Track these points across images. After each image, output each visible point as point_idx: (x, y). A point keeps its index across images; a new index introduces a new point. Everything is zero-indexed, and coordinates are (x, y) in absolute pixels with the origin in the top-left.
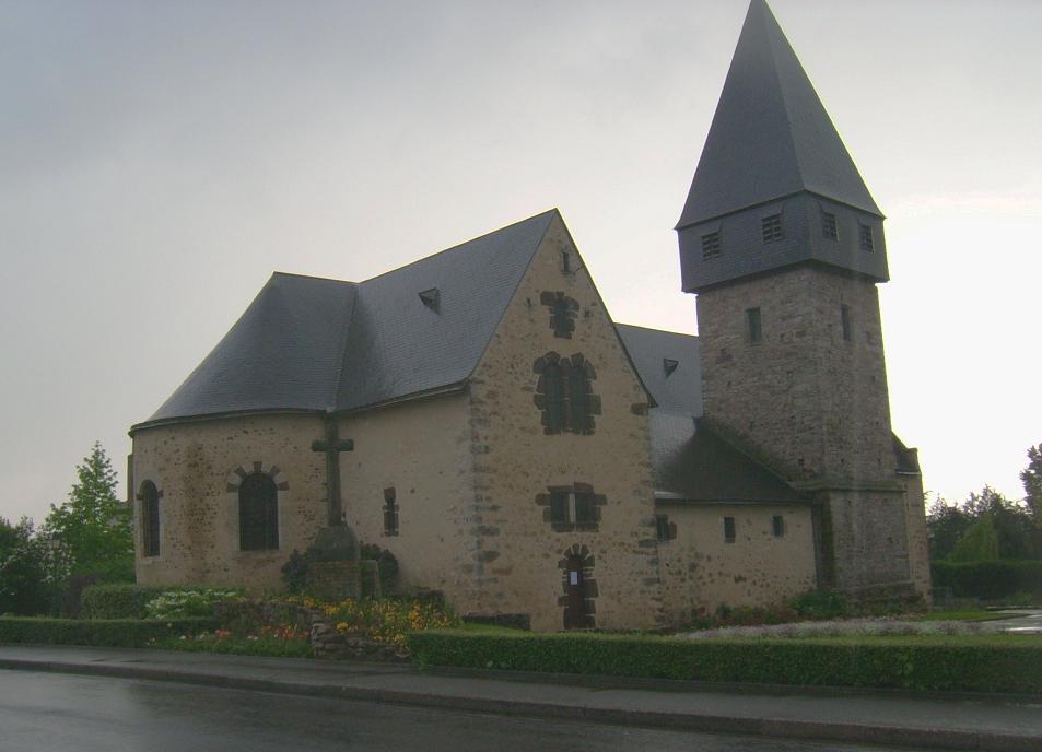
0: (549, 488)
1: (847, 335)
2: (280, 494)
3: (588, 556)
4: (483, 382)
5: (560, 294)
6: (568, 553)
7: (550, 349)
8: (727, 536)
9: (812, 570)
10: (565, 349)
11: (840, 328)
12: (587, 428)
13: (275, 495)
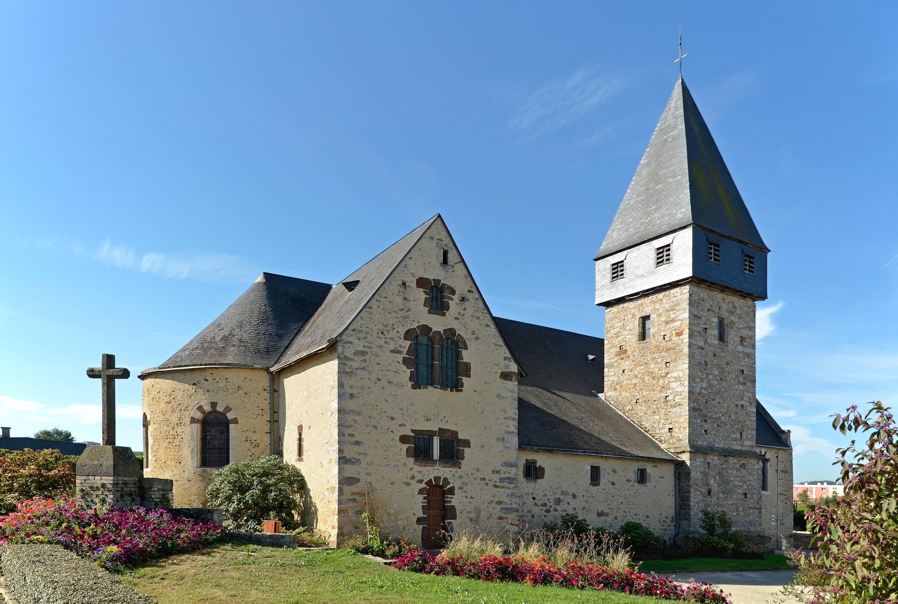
0: (413, 431)
1: (721, 338)
2: (232, 426)
3: (449, 487)
4: (350, 342)
5: (437, 281)
6: (429, 483)
7: (422, 322)
8: (592, 479)
9: (672, 513)
10: (438, 324)
11: (716, 332)
12: (457, 386)
13: (228, 427)
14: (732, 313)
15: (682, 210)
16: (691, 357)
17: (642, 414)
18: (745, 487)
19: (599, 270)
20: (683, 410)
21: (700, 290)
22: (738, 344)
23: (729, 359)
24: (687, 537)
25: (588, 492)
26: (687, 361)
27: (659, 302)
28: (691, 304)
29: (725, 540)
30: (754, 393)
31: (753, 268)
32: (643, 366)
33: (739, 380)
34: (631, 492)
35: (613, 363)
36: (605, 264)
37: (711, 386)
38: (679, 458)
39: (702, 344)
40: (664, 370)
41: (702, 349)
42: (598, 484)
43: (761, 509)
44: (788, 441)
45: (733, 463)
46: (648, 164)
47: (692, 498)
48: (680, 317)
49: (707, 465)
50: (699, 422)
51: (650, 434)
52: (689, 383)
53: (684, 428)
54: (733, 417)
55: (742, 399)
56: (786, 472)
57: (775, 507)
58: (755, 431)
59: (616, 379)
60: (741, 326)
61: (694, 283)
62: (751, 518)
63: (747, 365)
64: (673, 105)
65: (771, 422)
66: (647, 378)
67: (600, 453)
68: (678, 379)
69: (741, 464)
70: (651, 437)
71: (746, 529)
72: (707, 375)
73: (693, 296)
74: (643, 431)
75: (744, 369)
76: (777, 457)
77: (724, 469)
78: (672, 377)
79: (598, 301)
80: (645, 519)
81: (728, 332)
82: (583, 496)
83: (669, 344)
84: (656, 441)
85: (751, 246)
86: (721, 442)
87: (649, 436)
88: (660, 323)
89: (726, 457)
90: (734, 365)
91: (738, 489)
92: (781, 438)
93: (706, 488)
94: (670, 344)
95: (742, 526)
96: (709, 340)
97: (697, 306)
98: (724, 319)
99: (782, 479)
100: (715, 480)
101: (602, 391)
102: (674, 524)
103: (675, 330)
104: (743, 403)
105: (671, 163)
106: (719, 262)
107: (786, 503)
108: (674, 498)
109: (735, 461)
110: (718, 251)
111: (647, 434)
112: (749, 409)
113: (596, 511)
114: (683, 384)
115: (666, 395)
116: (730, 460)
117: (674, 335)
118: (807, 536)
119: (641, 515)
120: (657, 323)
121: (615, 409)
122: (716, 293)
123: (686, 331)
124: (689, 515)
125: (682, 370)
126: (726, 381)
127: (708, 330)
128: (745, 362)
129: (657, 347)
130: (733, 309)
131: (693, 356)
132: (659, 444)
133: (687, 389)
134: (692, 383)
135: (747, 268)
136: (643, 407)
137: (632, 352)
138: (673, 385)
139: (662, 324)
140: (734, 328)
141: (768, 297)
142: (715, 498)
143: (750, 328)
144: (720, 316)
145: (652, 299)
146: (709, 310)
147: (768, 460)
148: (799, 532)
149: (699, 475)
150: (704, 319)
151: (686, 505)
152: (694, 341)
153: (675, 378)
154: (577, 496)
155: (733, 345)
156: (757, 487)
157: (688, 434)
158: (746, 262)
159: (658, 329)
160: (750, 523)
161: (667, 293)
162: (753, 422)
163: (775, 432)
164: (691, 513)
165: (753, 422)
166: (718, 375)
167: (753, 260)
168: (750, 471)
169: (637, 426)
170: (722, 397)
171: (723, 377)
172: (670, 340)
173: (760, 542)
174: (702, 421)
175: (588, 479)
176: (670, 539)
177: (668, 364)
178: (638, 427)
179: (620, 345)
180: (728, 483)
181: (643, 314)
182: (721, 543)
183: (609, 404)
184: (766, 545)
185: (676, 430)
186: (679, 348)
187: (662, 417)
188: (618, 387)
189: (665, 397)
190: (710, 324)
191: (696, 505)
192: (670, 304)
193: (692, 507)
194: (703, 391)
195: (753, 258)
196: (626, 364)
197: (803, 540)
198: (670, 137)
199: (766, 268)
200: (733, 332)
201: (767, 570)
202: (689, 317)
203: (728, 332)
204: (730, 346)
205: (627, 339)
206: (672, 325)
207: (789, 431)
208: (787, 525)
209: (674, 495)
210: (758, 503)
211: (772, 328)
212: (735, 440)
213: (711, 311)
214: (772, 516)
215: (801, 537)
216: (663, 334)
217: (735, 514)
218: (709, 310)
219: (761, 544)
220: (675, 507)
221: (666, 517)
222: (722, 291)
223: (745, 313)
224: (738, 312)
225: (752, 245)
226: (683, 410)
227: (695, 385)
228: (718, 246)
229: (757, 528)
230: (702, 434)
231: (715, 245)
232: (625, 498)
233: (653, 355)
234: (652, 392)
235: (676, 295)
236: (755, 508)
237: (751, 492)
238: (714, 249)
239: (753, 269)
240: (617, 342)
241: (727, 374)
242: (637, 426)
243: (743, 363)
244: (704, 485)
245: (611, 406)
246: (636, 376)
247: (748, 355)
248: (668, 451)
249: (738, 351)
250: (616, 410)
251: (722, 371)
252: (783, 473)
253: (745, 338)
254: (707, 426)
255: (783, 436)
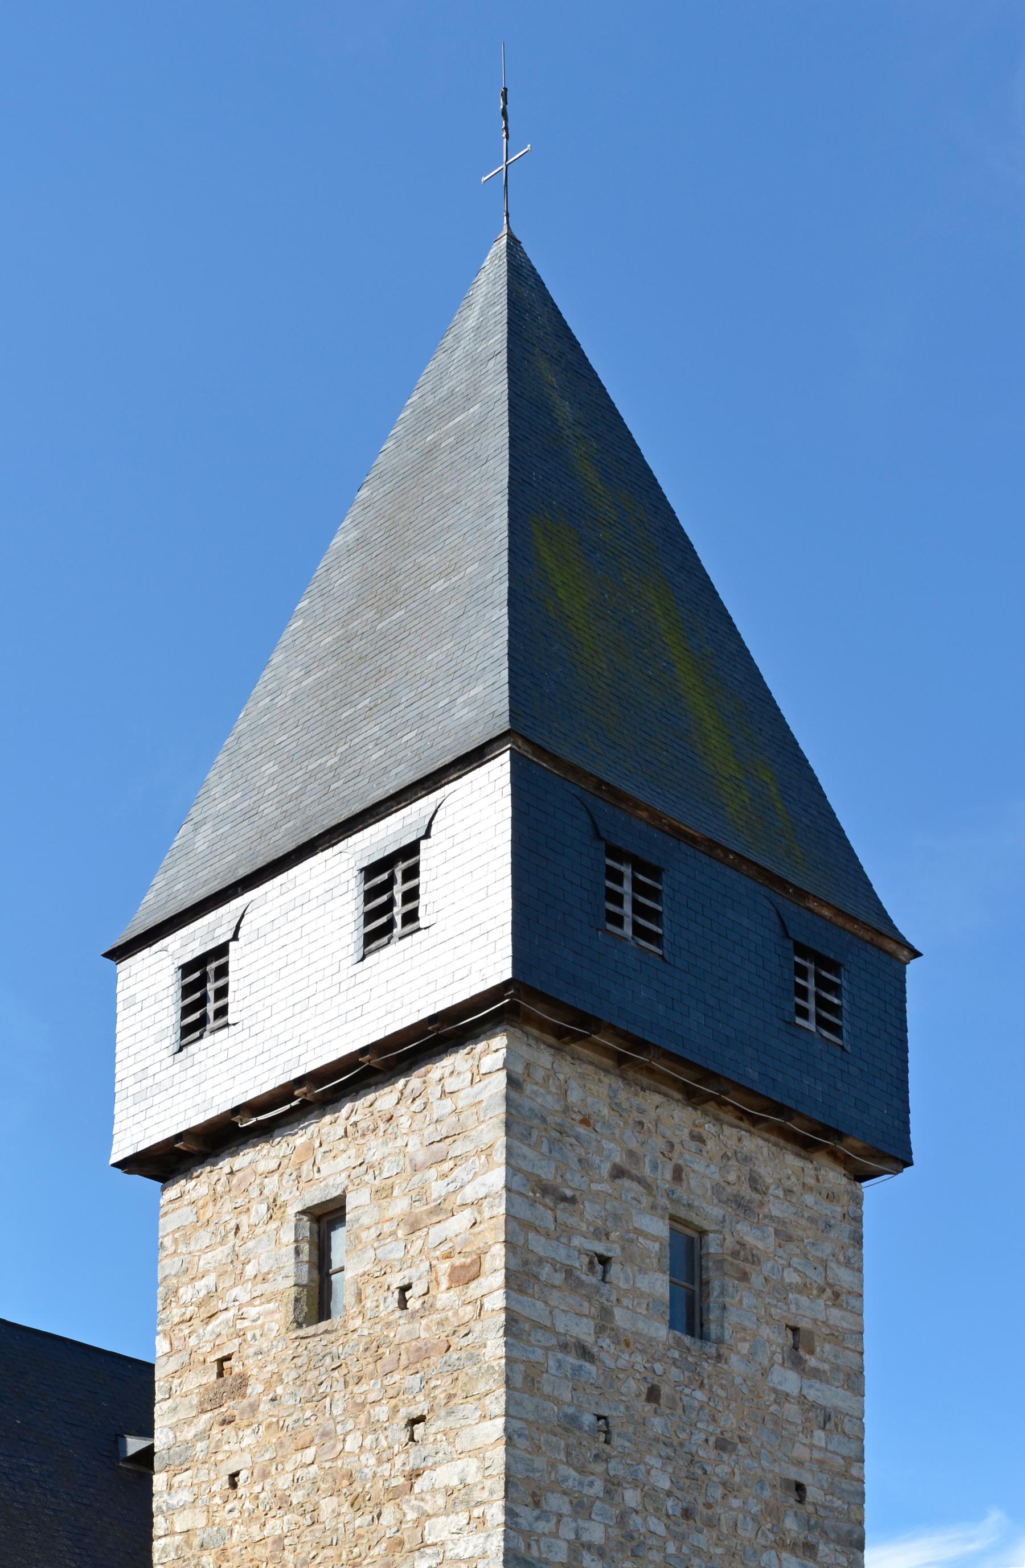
14: (742, 1206)
15: (472, 693)
16: (518, 1381)
21: (566, 1069)
22: (778, 1358)
23: (729, 1422)
26: (496, 1403)
27: (382, 1126)
31: (835, 1009)
33: (778, 1528)
35: (189, 1445)
39: (584, 1330)
40: (399, 1461)
41: (584, 1353)
46: (362, 542)
52: (509, 1512)
59: (201, 1521)
60: (791, 1277)
61: (535, 1032)
63: (821, 1463)
64: (471, 323)
72: (612, 1486)
73: (529, 1088)
75: (806, 1478)
78: (433, 1490)
81: (722, 1293)
83: (424, 1330)
88: (387, 1228)
90: (755, 1456)
94: (428, 1328)
96: (621, 1318)
97: (552, 1142)
98: (703, 1233)
103: (448, 1256)
106: (660, 946)
110: (653, 894)
114: (482, 1520)
117: (444, 1283)
120: (373, 1233)
122: (657, 1098)
123: (496, 1258)
125: (478, 1452)
126: (712, 1523)
127: (615, 1269)
128: (812, 1447)
129: (374, 1348)
131: (531, 1382)
134: (527, 1515)
135: (811, 1005)
137: (269, 1385)
138: (438, 1529)
139: (393, 1233)
140: (757, 1281)
141: (915, 1157)
143: (837, 1295)
144: (682, 1213)
145: (352, 1119)
150: (590, 1210)
152: (533, 1309)
153: (449, 1492)
155: (749, 1358)
158: (805, 998)
159: (377, 1261)
161: (414, 1081)
166: (669, 1494)
171: (700, 1507)
172: (427, 1308)
177: (419, 1429)
179: (219, 1355)
181: (315, 1196)
186: (464, 1342)
190: (627, 1243)
192: (426, 1132)
195: (834, 967)
200: (748, 1300)
202: (508, 1188)
203: (722, 1293)
204: (735, 1364)
206: (436, 1233)
216: (397, 1281)
218: (618, 1173)
222: (692, 1097)
223: (810, 1219)
224: (775, 1208)
225: (829, 905)
227: (542, 1526)
228: (655, 872)
233: (357, 1390)
235: (451, 1084)
238: (635, 882)
239: (839, 1016)
241: (718, 1493)
243: (801, 1452)
246: (283, 1502)
247: (828, 1418)
249: (775, 1390)
253: (810, 1333)
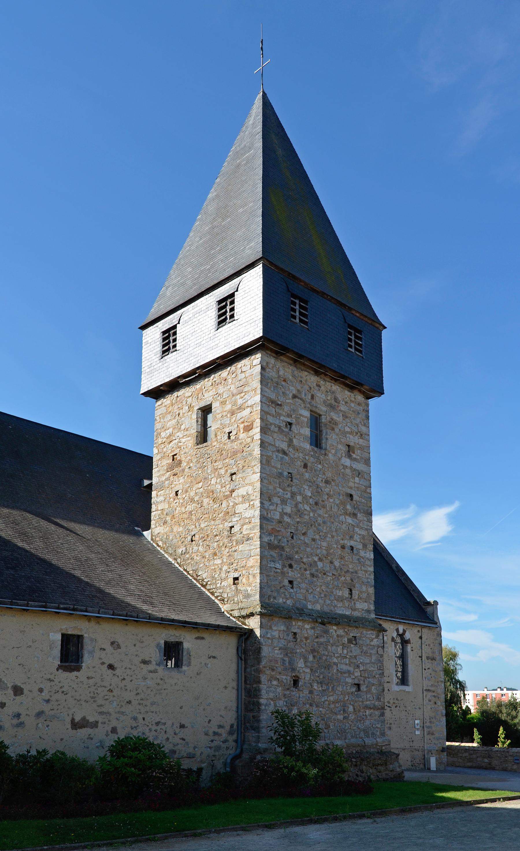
11: (307, 431)
14: (332, 407)
16: (264, 462)
17: (198, 558)
18: (357, 674)
19: (147, 343)
20: (253, 547)
21: (279, 364)
22: (344, 455)
23: (329, 475)
24: (252, 759)
25: (52, 683)
26: (258, 469)
27: (223, 382)
28: (263, 381)
29: (304, 763)
30: (370, 529)
31: (360, 345)
32: (201, 483)
33: (345, 509)
34: (149, 682)
35: (163, 482)
36: (154, 333)
37: (299, 513)
38: (245, 625)
39: (284, 446)
40: (228, 487)
41: (284, 453)
42: (78, 669)
43: (383, 708)
44: (435, 616)
45: (338, 636)
46: (217, 196)
47: (263, 692)
48: (249, 403)
49: (291, 637)
50: (278, 566)
51: (208, 590)
52: (261, 503)
53: (254, 576)
54: (337, 563)
55: (351, 537)
56: (433, 659)
57: (420, 708)
58: (373, 588)
59: (167, 506)
60: (347, 429)
61: (269, 353)
62: (367, 723)
63: (358, 488)
64: (251, 122)
65: (413, 590)
66: (206, 501)
67: (82, 611)
68: (246, 498)
69: (350, 637)
70: (209, 594)
71: (360, 742)
72: (293, 495)
73: (267, 370)
74: (200, 586)
75: (353, 493)
76: (421, 638)
77: (322, 644)
78: (238, 496)
79: (144, 390)
80: (178, 730)
82: (41, 690)
83: (236, 446)
84: (216, 601)
85: (358, 315)
86: (317, 602)
87: (207, 592)
88: (224, 414)
89: (324, 625)
90: (337, 485)
91: (346, 677)
92: (426, 613)
93: (290, 674)
94: (237, 445)
95: (352, 737)
97: (274, 387)
98: (320, 415)
99: (429, 669)
100: (305, 662)
101: (148, 527)
102: (234, 737)
103: (243, 423)
104: (352, 543)
105: (244, 189)
106: (307, 326)
107: (436, 703)
108: (235, 692)
109: (341, 632)
110: (305, 309)
111: (204, 590)
112: (362, 553)
113: (68, 720)
114: (253, 505)
115: (230, 525)
116: (331, 630)
117: (242, 431)
118: (466, 749)
119: (169, 723)
120: (220, 415)
121: (163, 553)
122: (306, 373)
123: (258, 423)
124: (259, 721)
125: (252, 484)
126: (324, 507)
127: (293, 427)
128: (355, 483)
129: (220, 451)
130: (333, 402)
131: (268, 462)
132: (220, 605)
133: (257, 513)
135: (353, 344)
136: (200, 547)
137: (188, 463)
138: (240, 508)
139: (226, 415)
140: (337, 430)
142: (306, 692)
143: (361, 435)
144: (314, 409)
145: (214, 380)
146: (294, 397)
147: (407, 642)
148: (463, 744)
149: (277, 654)
150: (286, 408)
151: (254, 704)
152: (269, 439)
153: (243, 497)
154: (26, 692)
156: (376, 674)
157: (259, 586)
159: (221, 424)
160: (366, 731)
161: (233, 368)
162: (370, 575)
163: (419, 604)
164: (261, 717)
165: (370, 575)
166: (311, 497)
167: (361, 335)
168: (365, 648)
169: (191, 578)
170: (319, 531)
171: (320, 502)
172: (237, 439)
173: (379, 762)
174: (284, 566)
175: (54, 658)
176: (225, 764)
177: (234, 476)
178: (193, 580)
179: (173, 454)
180: (328, 667)
181: (203, 404)
182: (297, 769)
183: (155, 546)
184: (391, 766)
185: (243, 580)
186: (248, 449)
187: (225, 560)
188: (168, 518)
189: (229, 529)
190: (297, 418)
191: (272, 702)
192: (236, 384)
193: (263, 707)
194: (286, 519)
195: (360, 332)
196: (179, 483)
197: (461, 755)
198: (244, 160)
199: (381, 351)
200: (334, 437)
201: (362, 817)
202: (261, 401)
204: (331, 456)
205: (181, 444)
206: (239, 415)
207: (436, 603)
208: (437, 735)
209: (236, 687)
210: (379, 699)
211: (450, 528)
212: (341, 599)
213: (299, 398)
214: (417, 722)
215: (458, 751)
216: (227, 430)
217: (340, 717)
218: (294, 397)
219: (382, 765)
220: (237, 707)
221: (220, 727)
222: (317, 373)
224: (343, 408)
225: (358, 312)
226: (253, 547)
227: (271, 507)
228: (306, 302)
229: (378, 739)
230: (284, 586)
231: (301, 300)
232: (137, 694)
233: (215, 464)
234: (213, 522)
235: (244, 369)
236: (375, 708)
237: (366, 682)
240: (169, 449)
242: (191, 578)
243: (351, 484)
244: (285, 669)
245: (159, 549)
246: (192, 500)
247: (359, 474)
248: (231, 615)
250: (166, 555)
251: (318, 491)
252: (430, 661)
253: (353, 447)
254: (291, 574)
255: (429, 610)
